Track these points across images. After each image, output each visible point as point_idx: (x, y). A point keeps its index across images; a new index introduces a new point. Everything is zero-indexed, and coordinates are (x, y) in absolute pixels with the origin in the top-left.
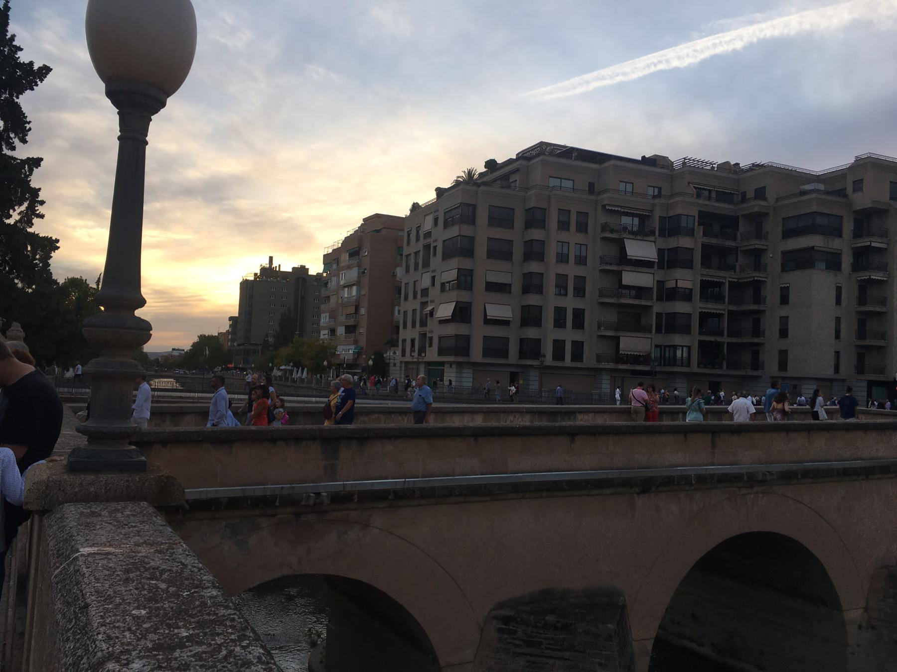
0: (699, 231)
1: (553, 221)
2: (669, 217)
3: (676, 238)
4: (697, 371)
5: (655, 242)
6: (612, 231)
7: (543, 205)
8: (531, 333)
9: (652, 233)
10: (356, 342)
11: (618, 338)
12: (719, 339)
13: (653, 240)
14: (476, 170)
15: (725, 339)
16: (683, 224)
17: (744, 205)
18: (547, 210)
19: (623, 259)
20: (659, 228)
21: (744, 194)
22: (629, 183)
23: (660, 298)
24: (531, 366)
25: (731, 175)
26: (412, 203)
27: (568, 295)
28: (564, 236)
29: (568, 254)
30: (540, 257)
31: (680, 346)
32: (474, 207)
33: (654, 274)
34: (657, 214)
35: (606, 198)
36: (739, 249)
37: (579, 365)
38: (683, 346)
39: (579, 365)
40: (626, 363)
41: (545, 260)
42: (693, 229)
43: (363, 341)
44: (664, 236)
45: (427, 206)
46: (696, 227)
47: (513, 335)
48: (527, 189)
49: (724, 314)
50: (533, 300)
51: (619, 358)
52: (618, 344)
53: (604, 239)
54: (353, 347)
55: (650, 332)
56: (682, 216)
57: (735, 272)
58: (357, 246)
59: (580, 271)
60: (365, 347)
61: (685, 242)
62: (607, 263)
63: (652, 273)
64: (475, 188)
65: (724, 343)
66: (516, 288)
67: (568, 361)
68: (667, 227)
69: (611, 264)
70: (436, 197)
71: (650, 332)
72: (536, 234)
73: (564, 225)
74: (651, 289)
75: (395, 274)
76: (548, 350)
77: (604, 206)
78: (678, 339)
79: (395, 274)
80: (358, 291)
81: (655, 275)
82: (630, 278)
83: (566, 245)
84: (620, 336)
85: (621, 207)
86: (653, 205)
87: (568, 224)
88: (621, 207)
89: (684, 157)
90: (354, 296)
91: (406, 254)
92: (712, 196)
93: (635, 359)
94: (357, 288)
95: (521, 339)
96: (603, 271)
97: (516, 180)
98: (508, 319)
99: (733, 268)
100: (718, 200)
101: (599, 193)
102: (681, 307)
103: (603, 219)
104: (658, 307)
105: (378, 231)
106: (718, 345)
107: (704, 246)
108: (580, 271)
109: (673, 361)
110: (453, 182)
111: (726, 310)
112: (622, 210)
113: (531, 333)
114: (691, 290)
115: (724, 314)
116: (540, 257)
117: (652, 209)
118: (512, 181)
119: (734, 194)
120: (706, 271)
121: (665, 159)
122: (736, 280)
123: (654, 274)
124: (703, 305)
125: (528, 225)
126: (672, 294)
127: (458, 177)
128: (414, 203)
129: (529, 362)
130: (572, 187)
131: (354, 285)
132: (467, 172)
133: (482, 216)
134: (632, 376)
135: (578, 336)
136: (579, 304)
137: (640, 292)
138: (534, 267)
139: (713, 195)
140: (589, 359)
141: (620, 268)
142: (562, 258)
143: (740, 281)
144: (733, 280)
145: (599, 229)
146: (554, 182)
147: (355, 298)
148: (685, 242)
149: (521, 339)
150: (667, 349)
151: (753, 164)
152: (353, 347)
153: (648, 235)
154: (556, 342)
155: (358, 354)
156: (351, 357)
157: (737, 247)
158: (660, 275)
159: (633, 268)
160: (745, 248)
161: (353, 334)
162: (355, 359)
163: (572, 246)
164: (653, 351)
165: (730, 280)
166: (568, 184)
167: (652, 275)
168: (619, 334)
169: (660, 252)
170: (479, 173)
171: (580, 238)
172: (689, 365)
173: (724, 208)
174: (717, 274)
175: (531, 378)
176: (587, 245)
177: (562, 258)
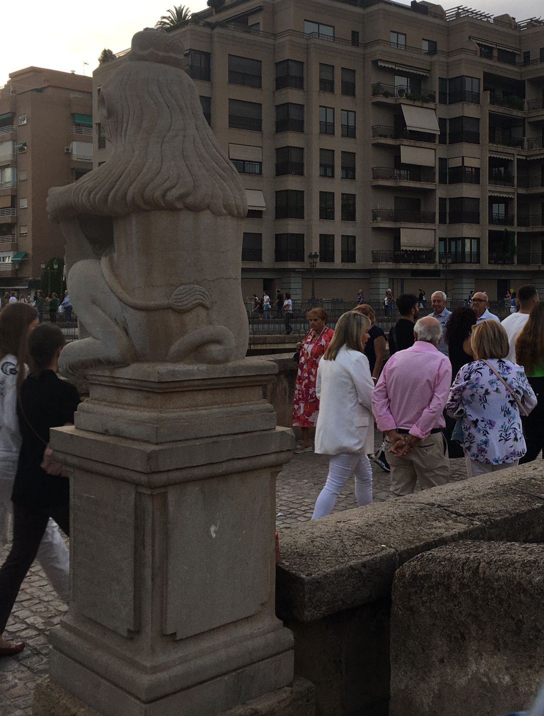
0: (486, 97)
1: (314, 77)
2: (449, 79)
3: (461, 105)
4: (488, 268)
5: (435, 110)
6: (386, 95)
7: (300, 58)
8: (292, 226)
9: (432, 98)
10: (15, 248)
11: (398, 231)
12: (509, 229)
13: (434, 107)
14: (187, 9)
15: (515, 229)
16: (468, 88)
17: (530, 68)
18: (305, 64)
19: (399, 129)
20: (439, 92)
21: (527, 55)
22: (402, 34)
23: (442, 181)
24: (293, 270)
25: (511, 31)
26: (103, 49)
27: (335, 177)
28: (328, 99)
29: (334, 123)
30: (299, 126)
31: (468, 238)
32: (208, 56)
33: (435, 149)
34: (438, 73)
35: (378, 52)
36: (526, 121)
37: (350, 266)
38: (471, 239)
39: (350, 266)
40: (406, 261)
41: (305, 129)
42: (479, 94)
43: (27, 245)
44: (445, 103)
45: (120, 57)
46: (481, 92)
47: (267, 230)
48: (275, 35)
49: (514, 199)
50: (292, 183)
51: (399, 255)
52: (397, 238)
53: (377, 105)
54: (11, 254)
55: (433, 222)
56: (467, 78)
57: (523, 148)
58: (9, 111)
59: (348, 145)
60: (30, 252)
61: (470, 110)
62: (381, 136)
63: (433, 149)
64: (207, 30)
65: (514, 233)
66: (269, 168)
67: (338, 263)
68: (448, 92)
69: (385, 136)
70: (131, 47)
71: (433, 222)
72: (293, 96)
73: (327, 86)
74: (433, 168)
75: (70, 151)
76: (314, 246)
77: (375, 63)
78: (467, 230)
79: (70, 151)
80: (15, 175)
81: (437, 150)
82: (411, 155)
83: (330, 112)
84: (399, 228)
85: (395, 63)
86: (432, 64)
87: (332, 83)
88: (395, 63)
89: (457, 6)
90: (8, 182)
91: (524, 51)
92: (494, 55)
93: (416, 256)
94: (13, 171)
95: (276, 235)
96: (377, 146)
97: (259, 23)
98: (260, 209)
99: (520, 143)
100: (500, 59)
101: (366, 46)
102: (468, 191)
103: (374, 78)
104: (441, 192)
105: (40, 91)
106: (508, 235)
107: (492, 116)
108: (348, 145)
109: (460, 257)
110: (157, 25)
111: (516, 194)
112: (397, 68)
113: (292, 226)
114: (477, 170)
115: (514, 199)
116: (299, 126)
117: (429, 69)
118: (251, 24)
119: (516, 53)
120: (494, 147)
121: (439, 7)
122: (524, 158)
123: (435, 149)
124: (493, 189)
125: (281, 83)
126: (457, 175)
127: (164, 18)
128: (105, 51)
129: (291, 265)
130: (332, 35)
131: (7, 166)
132: (175, 12)
133: (220, 69)
134: (413, 278)
135: (349, 229)
136: (348, 188)
137: (417, 172)
138: (292, 139)
139: (495, 53)
140: (363, 259)
141: (397, 142)
142: (327, 129)
143: (528, 159)
144: (521, 157)
145: (370, 91)
146: (310, 28)
147: (9, 185)
148: (470, 110)
149: (276, 235)
150: (453, 244)
151: (531, 19)
152: (11, 254)
153: (427, 101)
154: (323, 236)
155: (20, 264)
156: (10, 269)
157: (524, 118)
158: (442, 151)
159: (412, 142)
160: (532, 120)
161: (10, 237)
162: (15, 272)
163: (338, 112)
164: (437, 246)
165: (519, 157)
166: (327, 31)
167: (434, 151)
168: (398, 225)
169: (442, 122)
170: (192, 14)
171: (347, 102)
172: (478, 262)
173: (508, 71)
174: (505, 151)
175: (292, 286)
176: (355, 112)
177: (327, 129)
